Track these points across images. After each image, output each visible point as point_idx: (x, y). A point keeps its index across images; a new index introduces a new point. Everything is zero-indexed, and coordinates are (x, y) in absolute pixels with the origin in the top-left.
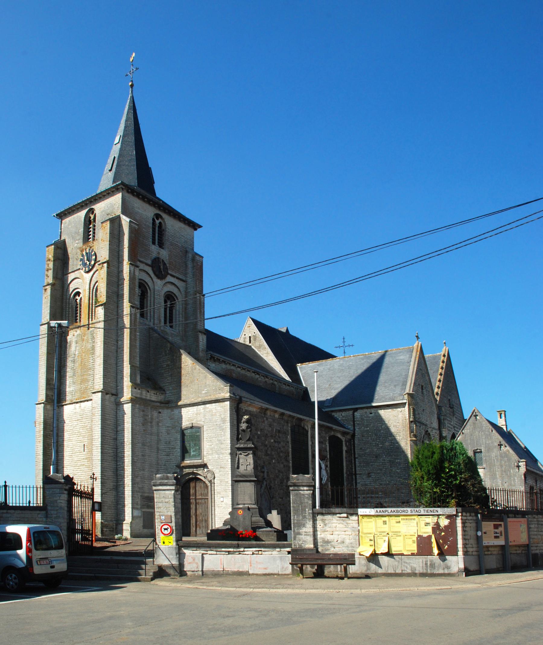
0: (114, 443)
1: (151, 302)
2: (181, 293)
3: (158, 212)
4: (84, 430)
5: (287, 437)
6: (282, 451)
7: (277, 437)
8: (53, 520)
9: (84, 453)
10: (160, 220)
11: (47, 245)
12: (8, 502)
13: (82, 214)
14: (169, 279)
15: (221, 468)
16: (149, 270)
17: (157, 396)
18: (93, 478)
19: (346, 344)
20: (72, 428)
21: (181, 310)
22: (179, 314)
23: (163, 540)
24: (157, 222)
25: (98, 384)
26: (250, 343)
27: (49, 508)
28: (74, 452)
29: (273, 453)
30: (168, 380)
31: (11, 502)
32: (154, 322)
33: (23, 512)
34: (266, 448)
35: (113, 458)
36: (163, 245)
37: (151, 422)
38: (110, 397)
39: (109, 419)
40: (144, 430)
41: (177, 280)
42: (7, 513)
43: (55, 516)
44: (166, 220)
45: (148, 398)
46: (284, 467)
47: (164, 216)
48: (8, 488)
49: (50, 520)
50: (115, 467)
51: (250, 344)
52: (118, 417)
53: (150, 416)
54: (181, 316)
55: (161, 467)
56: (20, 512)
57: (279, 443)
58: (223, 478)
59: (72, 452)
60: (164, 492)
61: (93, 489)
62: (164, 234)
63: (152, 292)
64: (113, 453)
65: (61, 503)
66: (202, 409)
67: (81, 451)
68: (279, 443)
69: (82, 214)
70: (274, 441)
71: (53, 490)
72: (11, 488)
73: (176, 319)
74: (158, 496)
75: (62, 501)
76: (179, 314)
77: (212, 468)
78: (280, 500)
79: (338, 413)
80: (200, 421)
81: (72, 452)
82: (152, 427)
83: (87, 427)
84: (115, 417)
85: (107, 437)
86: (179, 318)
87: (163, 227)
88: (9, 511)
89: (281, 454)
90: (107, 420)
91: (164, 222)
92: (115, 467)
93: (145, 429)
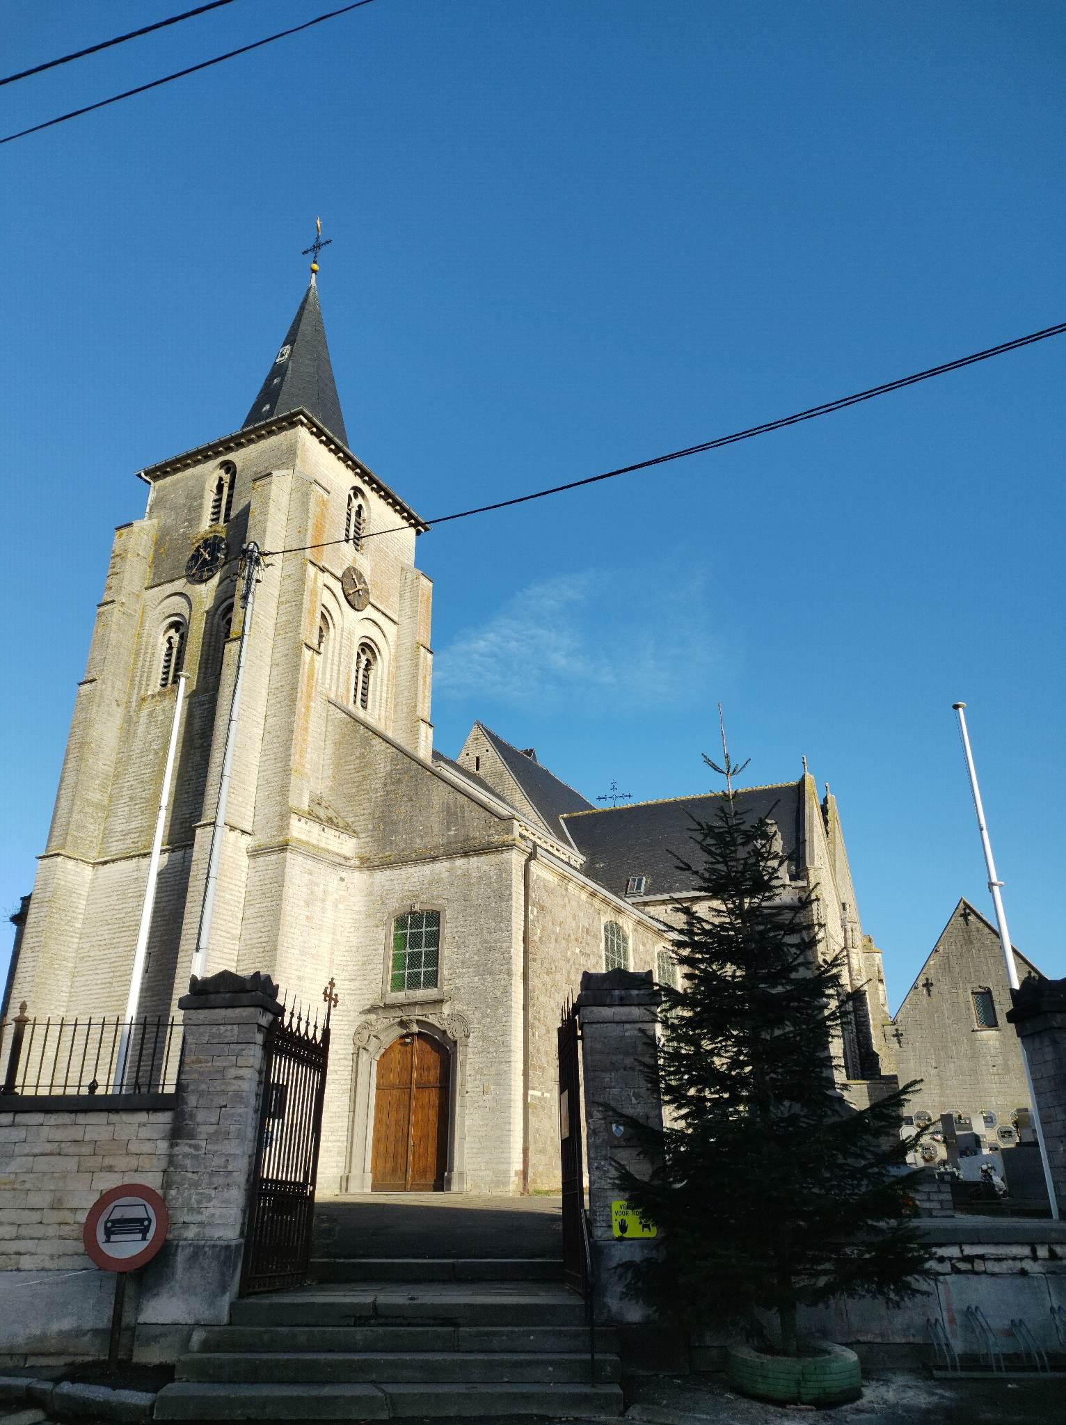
2: (388, 645)
3: (358, 482)
5: (598, 946)
8: (197, 1147)
10: (360, 500)
11: (117, 526)
12: (19, 1081)
14: (369, 612)
16: (337, 587)
17: (339, 841)
18: (331, 999)
19: (618, 793)
20: (123, 915)
21: (385, 679)
22: (381, 686)
23: (619, 1218)
26: (477, 769)
27: (192, 1100)
28: (118, 974)
31: (31, 1080)
32: (337, 691)
33: (81, 1118)
37: (323, 901)
38: (237, 837)
40: (307, 916)
42: (13, 1125)
43: (212, 1129)
45: (322, 845)
48: (28, 1029)
49: (187, 1150)
51: (478, 772)
53: (322, 886)
56: (66, 1118)
59: (111, 974)
61: (326, 1032)
63: (339, 631)
65: (240, 1078)
66: (444, 870)
70: (580, 951)
71: (215, 1029)
72: (40, 1030)
75: (241, 1072)
76: (381, 686)
77: (465, 1008)
79: (658, 908)
80: (439, 897)
81: (111, 974)
82: (323, 910)
85: (219, 932)
88: (21, 1118)
90: (224, 891)
91: (368, 505)
93: (309, 914)
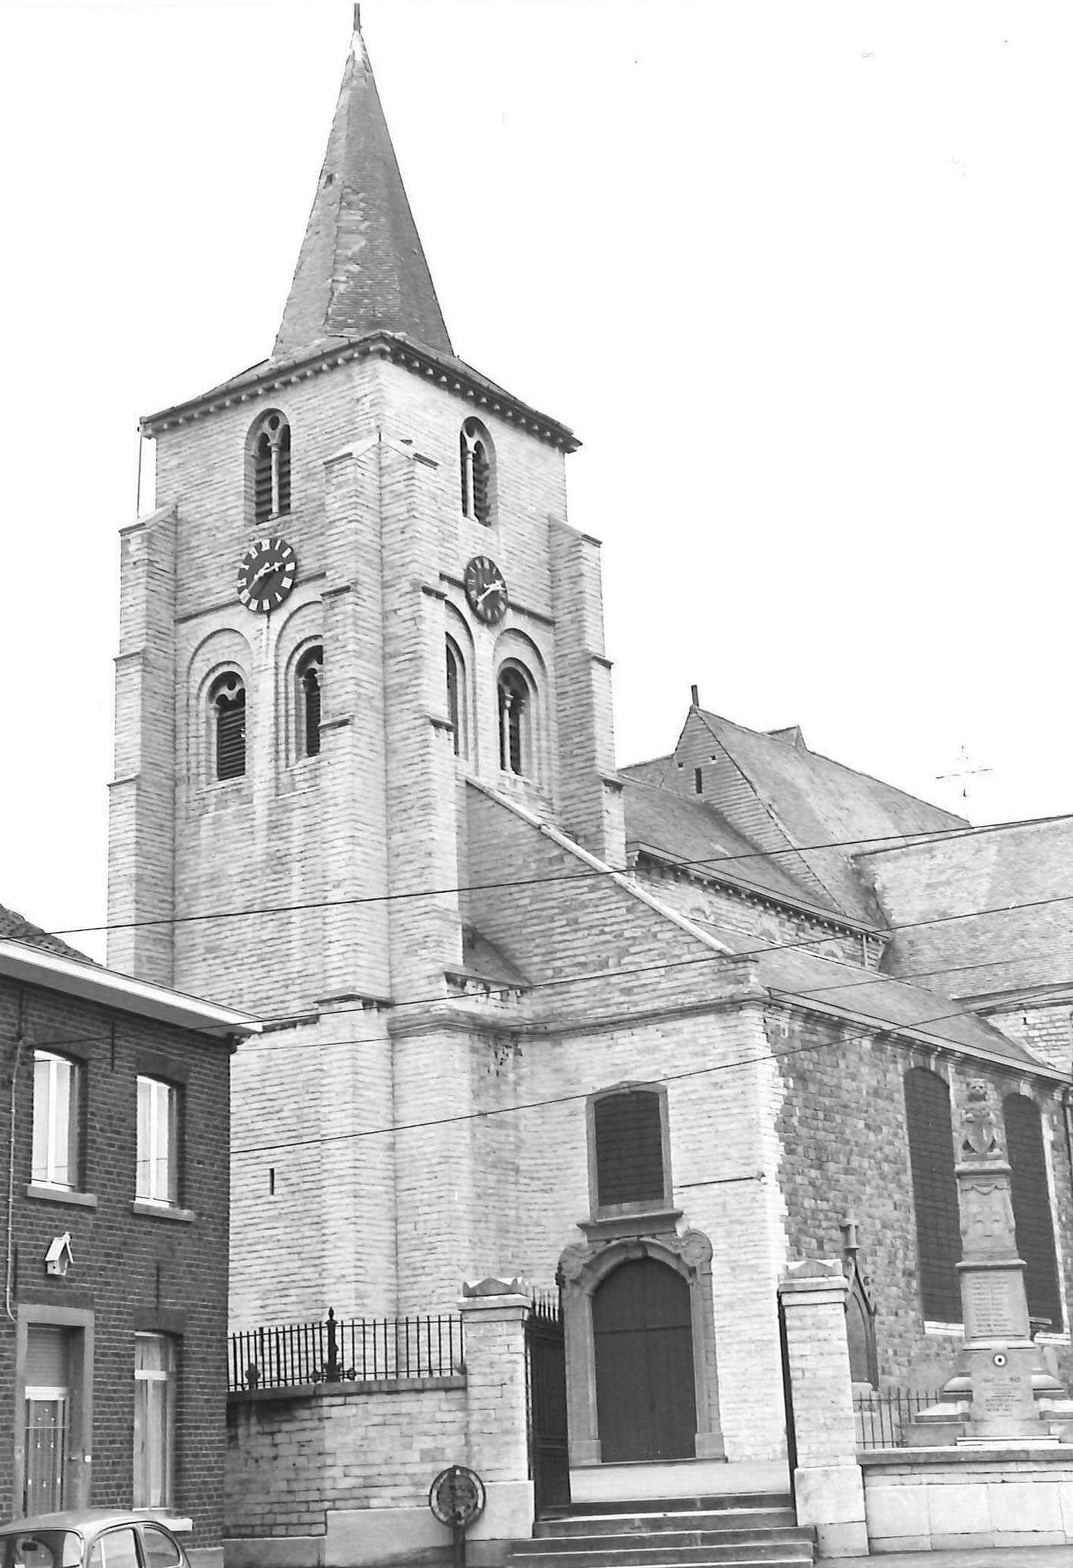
0: (388, 1160)
1: (465, 700)
3: (471, 412)
4: (271, 1123)
6: (886, 1159)
7: (872, 1110)
9: (272, 1198)
13: (244, 419)
15: (732, 1222)
24: (471, 443)
25: (337, 972)
29: (866, 1164)
30: (538, 946)
34: (848, 1148)
35: (385, 1210)
36: (487, 514)
39: (374, 1084)
41: (531, 621)
44: (493, 436)
46: (895, 1208)
47: (490, 423)
50: (393, 1238)
52: (397, 1074)
54: (543, 733)
55: (527, 1232)
57: (878, 1130)
58: (742, 1257)
60: (813, 1309)
62: (487, 479)
64: (387, 1193)
67: (260, 1193)
68: (878, 1130)
69: (244, 419)
73: (529, 746)
74: (797, 1323)
78: (892, 1318)
83: (281, 1111)
84: (387, 1074)
86: (538, 740)
87: (487, 457)
89: (886, 1167)
92: (393, 1238)
